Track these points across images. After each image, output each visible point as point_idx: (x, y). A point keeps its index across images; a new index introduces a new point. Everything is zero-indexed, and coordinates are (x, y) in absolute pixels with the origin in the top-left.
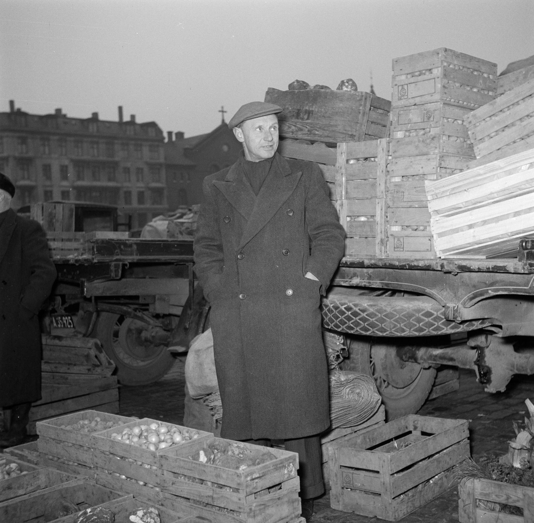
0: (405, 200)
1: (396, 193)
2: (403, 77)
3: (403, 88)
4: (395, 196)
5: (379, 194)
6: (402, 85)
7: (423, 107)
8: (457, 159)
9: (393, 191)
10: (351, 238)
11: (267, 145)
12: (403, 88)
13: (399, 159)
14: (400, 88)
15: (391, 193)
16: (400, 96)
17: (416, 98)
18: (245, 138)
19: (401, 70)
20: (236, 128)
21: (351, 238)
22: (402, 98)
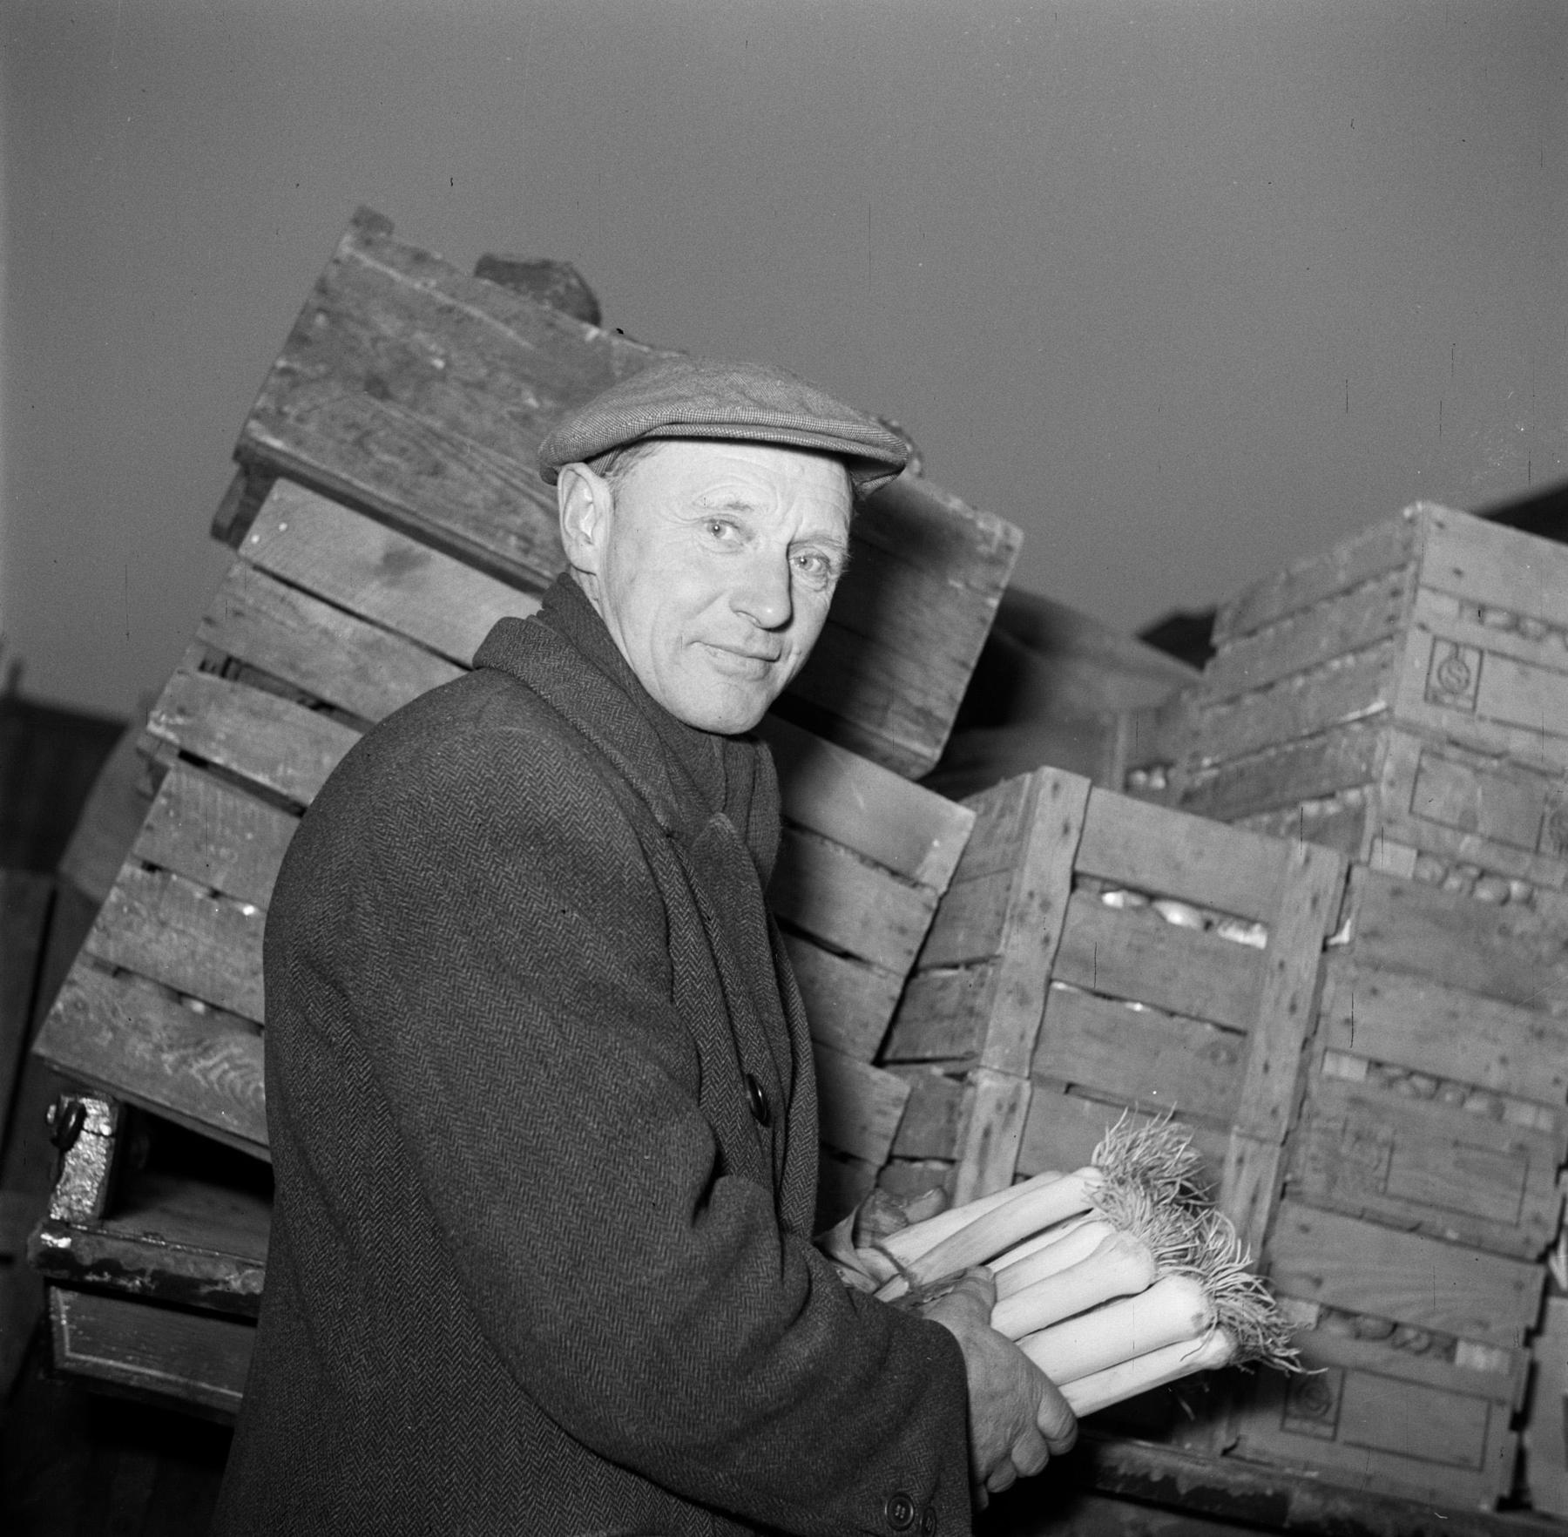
0: (1392, 1188)
1: (1349, 1138)
2: (1448, 607)
3: (1455, 656)
4: (1344, 1150)
5: (1249, 1113)
6: (1456, 645)
7: (1542, 786)
8: (386, 578)
9: (1336, 1126)
10: (703, 1200)
11: (737, 642)
12: (1455, 656)
13: (1392, 978)
14: (1443, 651)
15: (1325, 1131)
16: (1434, 681)
17: (1515, 733)
18: (612, 546)
19: (1458, 573)
20: (582, 469)
21: (703, 1200)
22: (1448, 699)
